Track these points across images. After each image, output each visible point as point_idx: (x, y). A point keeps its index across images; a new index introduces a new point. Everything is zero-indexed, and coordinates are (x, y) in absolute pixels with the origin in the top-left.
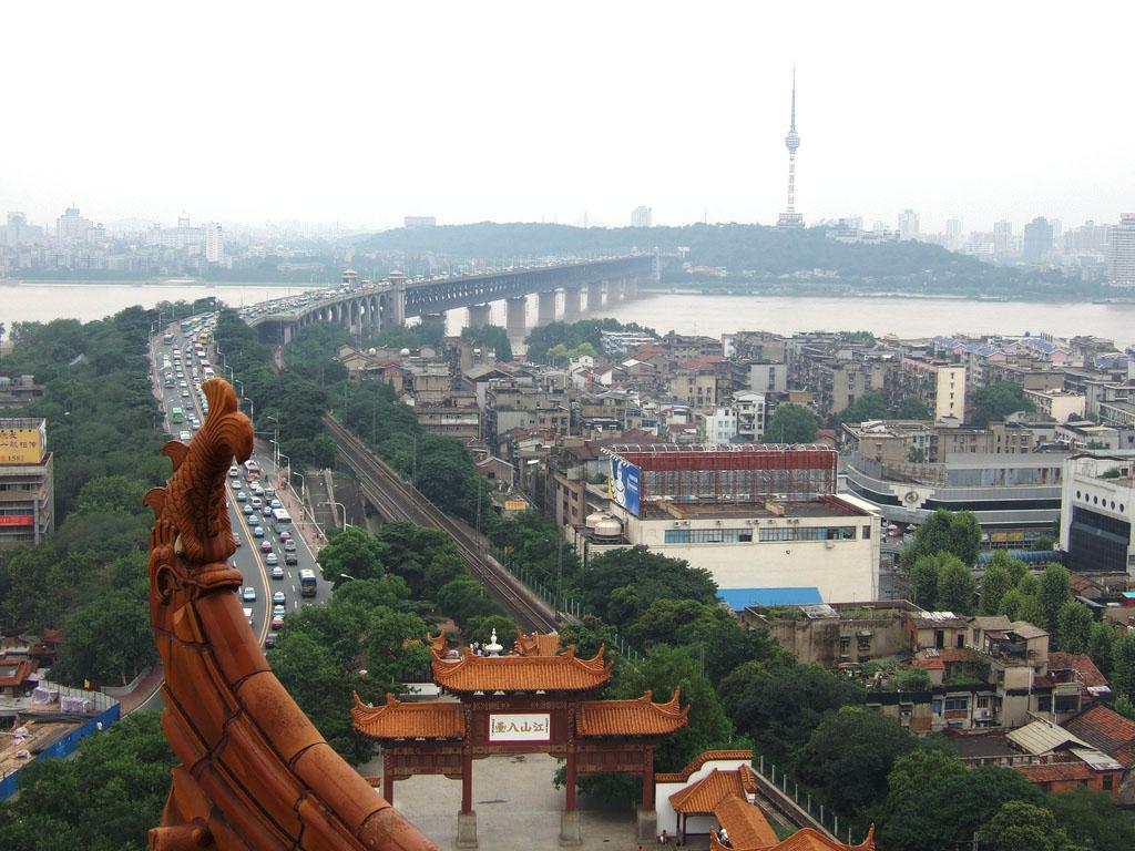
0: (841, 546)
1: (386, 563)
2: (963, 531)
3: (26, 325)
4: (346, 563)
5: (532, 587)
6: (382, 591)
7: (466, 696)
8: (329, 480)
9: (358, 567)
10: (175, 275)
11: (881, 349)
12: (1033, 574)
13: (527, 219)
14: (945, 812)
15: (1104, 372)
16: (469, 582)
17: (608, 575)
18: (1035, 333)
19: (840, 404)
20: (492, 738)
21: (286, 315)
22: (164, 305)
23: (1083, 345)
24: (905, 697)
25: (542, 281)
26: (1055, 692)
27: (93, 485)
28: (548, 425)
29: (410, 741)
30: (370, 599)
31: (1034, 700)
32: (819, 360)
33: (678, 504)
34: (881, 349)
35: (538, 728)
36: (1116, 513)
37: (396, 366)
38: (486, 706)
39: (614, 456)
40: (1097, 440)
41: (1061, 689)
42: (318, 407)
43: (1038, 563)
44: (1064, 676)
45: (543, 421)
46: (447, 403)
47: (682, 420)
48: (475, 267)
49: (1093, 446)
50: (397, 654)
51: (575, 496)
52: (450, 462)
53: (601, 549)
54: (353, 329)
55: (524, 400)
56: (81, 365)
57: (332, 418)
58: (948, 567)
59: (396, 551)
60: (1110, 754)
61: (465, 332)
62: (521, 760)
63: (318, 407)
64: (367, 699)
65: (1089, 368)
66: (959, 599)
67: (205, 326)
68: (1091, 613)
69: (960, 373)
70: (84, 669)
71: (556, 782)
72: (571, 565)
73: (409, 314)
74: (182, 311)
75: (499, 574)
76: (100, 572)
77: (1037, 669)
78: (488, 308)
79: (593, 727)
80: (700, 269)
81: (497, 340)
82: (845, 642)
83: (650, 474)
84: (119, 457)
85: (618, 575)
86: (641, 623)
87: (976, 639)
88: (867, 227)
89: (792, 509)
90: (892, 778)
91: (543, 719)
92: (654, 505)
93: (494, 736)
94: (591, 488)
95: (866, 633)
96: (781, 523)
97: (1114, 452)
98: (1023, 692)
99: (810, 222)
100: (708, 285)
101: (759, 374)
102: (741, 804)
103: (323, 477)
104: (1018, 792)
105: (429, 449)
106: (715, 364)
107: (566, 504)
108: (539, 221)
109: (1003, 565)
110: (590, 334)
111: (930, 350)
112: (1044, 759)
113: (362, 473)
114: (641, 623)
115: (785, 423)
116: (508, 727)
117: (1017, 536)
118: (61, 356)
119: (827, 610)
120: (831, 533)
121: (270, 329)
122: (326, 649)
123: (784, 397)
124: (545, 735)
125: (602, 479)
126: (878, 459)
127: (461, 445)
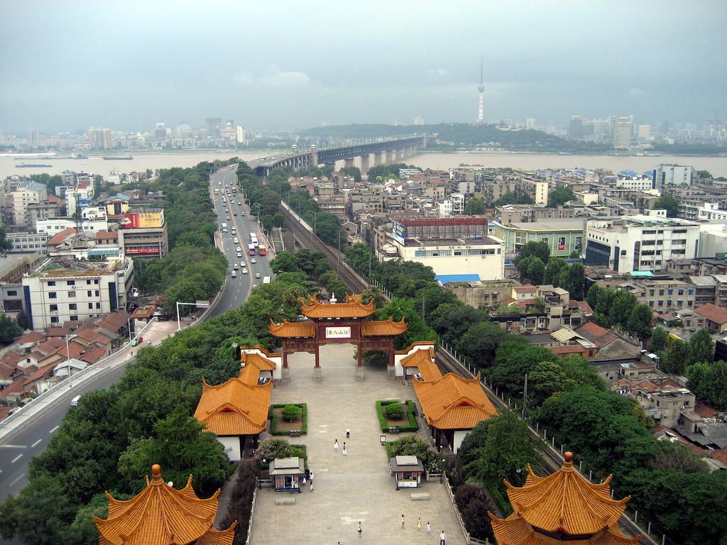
0: (489, 257)
7: (316, 320)
15: (607, 184)
19: (496, 196)
24: (510, 319)
26: (571, 317)
29: (293, 338)
31: (563, 320)
35: (346, 333)
36: (604, 243)
37: (311, 185)
41: (574, 316)
47: (430, 205)
49: (600, 215)
51: (382, 237)
53: (387, 259)
54: (296, 170)
55: (364, 198)
56: (181, 186)
69: (546, 185)
74: (225, 164)
77: (564, 307)
89: (469, 241)
91: (348, 329)
93: (328, 336)
94: (388, 234)
96: (464, 247)
98: (558, 317)
101: (463, 186)
107: (378, 241)
116: (333, 332)
120: (484, 252)
121: (260, 171)
123: (472, 195)
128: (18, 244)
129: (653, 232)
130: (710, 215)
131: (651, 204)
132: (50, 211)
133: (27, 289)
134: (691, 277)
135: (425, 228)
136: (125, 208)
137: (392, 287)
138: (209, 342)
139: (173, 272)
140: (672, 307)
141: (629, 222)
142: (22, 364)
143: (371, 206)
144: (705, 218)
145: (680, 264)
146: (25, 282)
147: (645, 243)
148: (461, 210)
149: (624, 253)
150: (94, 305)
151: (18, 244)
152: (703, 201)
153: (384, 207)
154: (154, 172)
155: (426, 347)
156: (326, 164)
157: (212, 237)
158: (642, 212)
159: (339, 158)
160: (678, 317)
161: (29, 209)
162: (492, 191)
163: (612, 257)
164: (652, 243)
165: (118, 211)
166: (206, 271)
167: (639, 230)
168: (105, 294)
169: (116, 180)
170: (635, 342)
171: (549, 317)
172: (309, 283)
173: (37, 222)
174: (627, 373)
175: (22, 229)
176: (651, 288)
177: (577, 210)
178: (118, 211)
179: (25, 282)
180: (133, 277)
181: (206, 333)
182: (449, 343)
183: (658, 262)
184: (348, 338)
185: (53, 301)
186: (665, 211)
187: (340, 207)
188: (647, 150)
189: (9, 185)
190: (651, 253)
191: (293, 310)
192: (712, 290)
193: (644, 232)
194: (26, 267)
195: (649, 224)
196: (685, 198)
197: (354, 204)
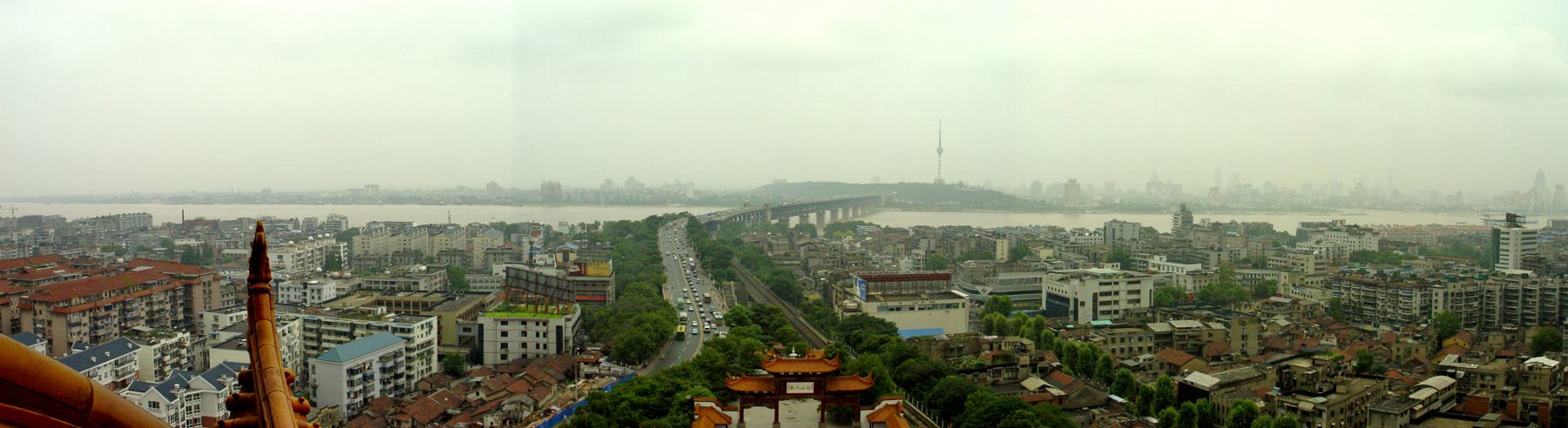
0: (953, 311)
1: (753, 320)
2: (1004, 304)
3: (609, 222)
4: (735, 320)
5: (819, 330)
6: (750, 331)
7: (777, 375)
8: (732, 286)
9: (741, 321)
10: (672, 203)
11: (975, 232)
12: (1031, 320)
13: (826, 180)
14: (986, 416)
15: (1060, 240)
16: (789, 328)
17: (850, 325)
18: (1033, 225)
19: (957, 255)
20: (788, 392)
21: (719, 219)
22: (667, 215)
23: (1053, 229)
24: (976, 371)
25: (833, 205)
26: (1039, 365)
27: (631, 286)
28: (831, 264)
29: (751, 393)
30: (744, 334)
31: (1030, 369)
32: (949, 237)
33: (883, 296)
34: (975, 232)
35: (809, 388)
36: (1064, 295)
38: (785, 379)
39: (855, 276)
40: (1058, 266)
41: (1041, 364)
42: (729, 256)
43: (1033, 315)
44: (1042, 359)
45: (828, 262)
46: (786, 255)
47: (890, 261)
48: (801, 199)
49: (1055, 269)
50: (752, 357)
51: (840, 293)
52: (785, 279)
53: (847, 315)
54: (748, 225)
56: (630, 238)
57: (735, 260)
58: (997, 318)
59: (757, 315)
60: (1062, 389)
61: (797, 226)
62: (804, 401)
63: (729, 256)
64: (733, 375)
65: (1055, 238)
66: (1002, 331)
67: (684, 223)
68: (1054, 334)
69: (1006, 242)
70: (622, 357)
71: (818, 410)
72: (835, 322)
73: (772, 219)
74: (673, 217)
75: (804, 325)
76: (630, 320)
77: (1031, 357)
78: (808, 216)
79: (833, 387)
80: (902, 201)
81: (812, 230)
82: (952, 350)
83: (871, 284)
84: (643, 274)
85: (856, 325)
86: (864, 345)
87: (1005, 346)
88: (972, 185)
89: (932, 296)
90: (967, 404)
91: (811, 384)
92: (873, 296)
93: (789, 391)
94: (847, 290)
95: (961, 345)
96: (928, 302)
97: (1065, 271)
98: (1026, 366)
99: (947, 182)
100: (904, 207)
101: (923, 243)
102: (898, 418)
103: (730, 285)
104: (1021, 406)
105: (776, 274)
106: (905, 239)
107: (837, 296)
108: (832, 181)
109: (1020, 316)
110: (852, 227)
111: (994, 233)
112: (1034, 392)
113: (746, 283)
114: (864, 345)
115: (932, 261)
116: (794, 388)
117: (1026, 304)
118: (622, 235)
119: (945, 337)
120: (948, 306)
121: (711, 225)
122: (723, 354)
123: (934, 252)
124: (812, 391)
125: (851, 286)
126: (972, 276)
127: (790, 272)
128: (475, 284)
129: (1109, 284)
130: (1159, 267)
131: (1105, 258)
132: (506, 256)
133: (481, 326)
134: (1149, 325)
135: (879, 283)
136: (573, 257)
137: (855, 342)
138: (661, 392)
139: (620, 321)
140: (1133, 353)
141: (1086, 275)
142: (472, 396)
143: (828, 262)
144: (1155, 269)
145: (1136, 312)
146: (480, 320)
147: (1103, 294)
148: (922, 266)
149: (1083, 304)
150: (541, 346)
151: (475, 284)
152: (1152, 254)
153: (842, 263)
154: (602, 223)
155: (894, 402)
156: (780, 220)
157: (660, 288)
158: (1095, 266)
159: (793, 215)
160: (1141, 361)
161: (487, 254)
162: (953, 248)
163: (1071, 308)
164: (1108, 294)
165: (566, 259)
166: (656, 322)
167: (1096, 283)
168: (552, 337)
169: (566, 231)
170: (1102, 387)
171: (1018, 366)
172: (764, 337)
173: (494, 266)
174: (1098, 418)
175: (479, 272)
176: (1113, 336)
177: (1034, 264)
178: (566, 259)
179: (480, 320)
180: (579, 323)
181: (657, 384)
182: (917, 397)
183: (1116, 312)
184: (811, 394)
185: (504, 339)
186: (1119, 264)
187: (796, 262)
188: (1094, 208)
189: (469, 231)
190: (1108, 303)
191: (751, 364)
192: (1168, 335)
193: (1101, 284)
194: (482, 307)
195: (1104, 275)
196: (1135, 252)
197: (809, 260)
